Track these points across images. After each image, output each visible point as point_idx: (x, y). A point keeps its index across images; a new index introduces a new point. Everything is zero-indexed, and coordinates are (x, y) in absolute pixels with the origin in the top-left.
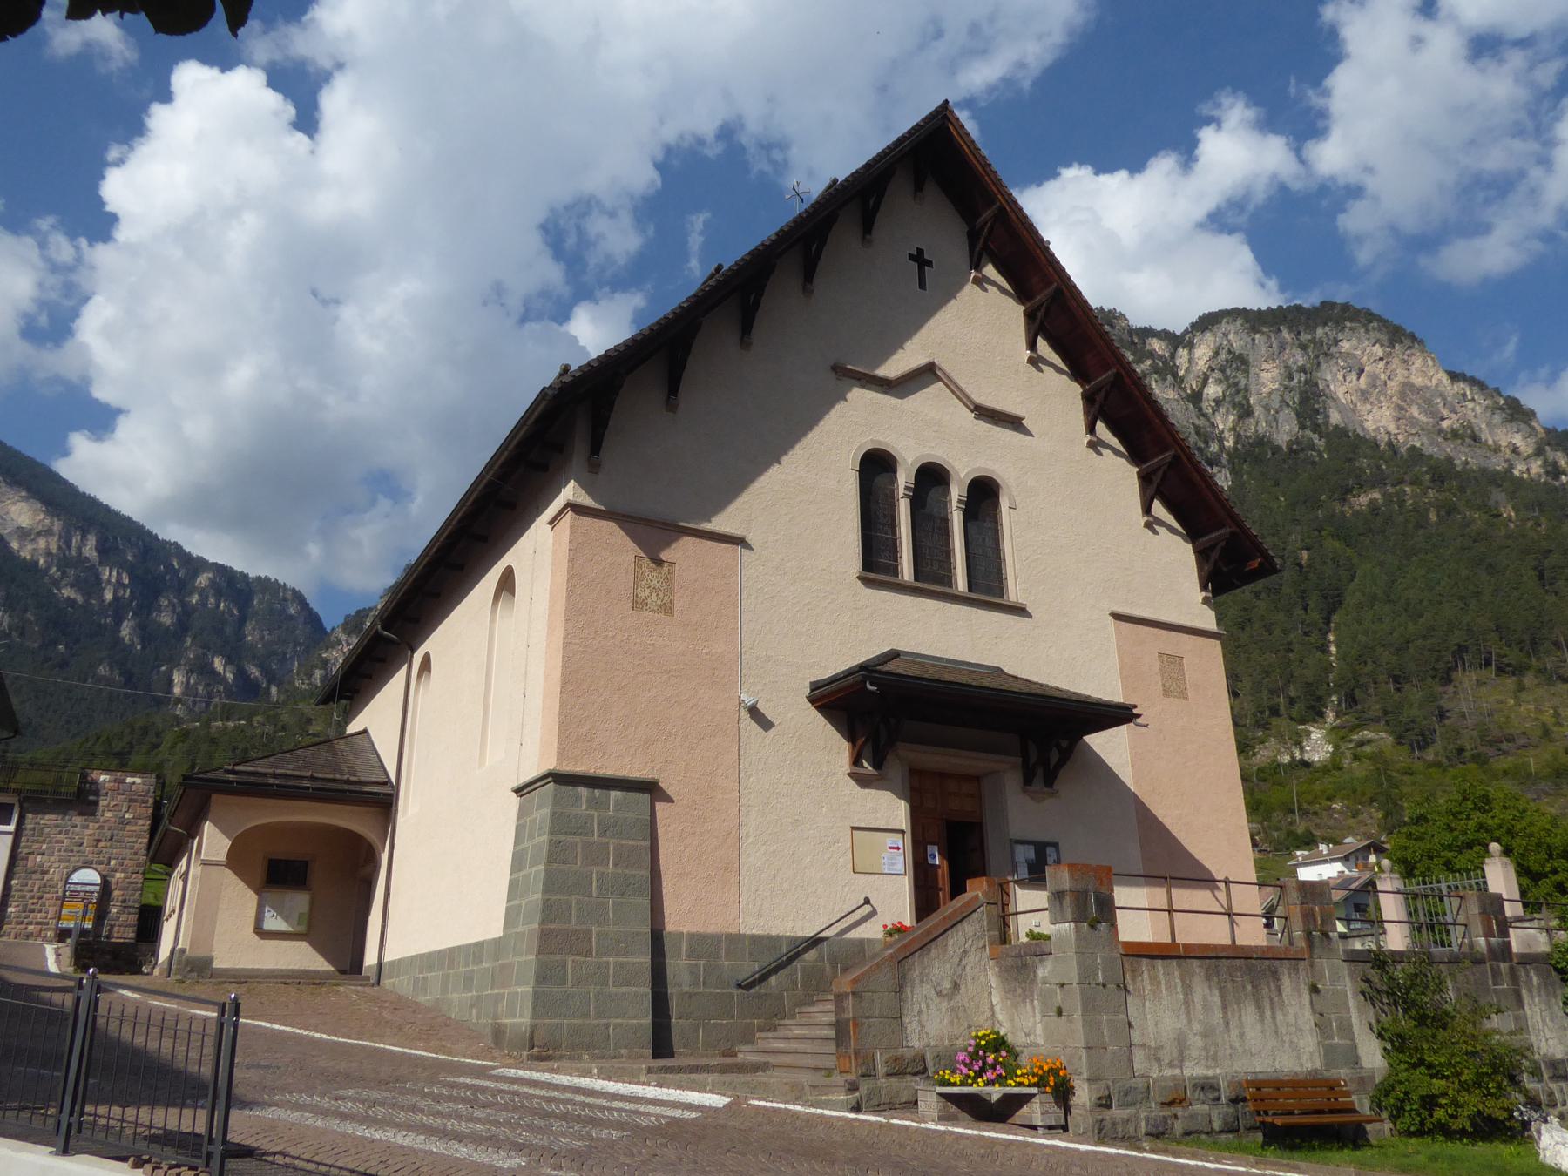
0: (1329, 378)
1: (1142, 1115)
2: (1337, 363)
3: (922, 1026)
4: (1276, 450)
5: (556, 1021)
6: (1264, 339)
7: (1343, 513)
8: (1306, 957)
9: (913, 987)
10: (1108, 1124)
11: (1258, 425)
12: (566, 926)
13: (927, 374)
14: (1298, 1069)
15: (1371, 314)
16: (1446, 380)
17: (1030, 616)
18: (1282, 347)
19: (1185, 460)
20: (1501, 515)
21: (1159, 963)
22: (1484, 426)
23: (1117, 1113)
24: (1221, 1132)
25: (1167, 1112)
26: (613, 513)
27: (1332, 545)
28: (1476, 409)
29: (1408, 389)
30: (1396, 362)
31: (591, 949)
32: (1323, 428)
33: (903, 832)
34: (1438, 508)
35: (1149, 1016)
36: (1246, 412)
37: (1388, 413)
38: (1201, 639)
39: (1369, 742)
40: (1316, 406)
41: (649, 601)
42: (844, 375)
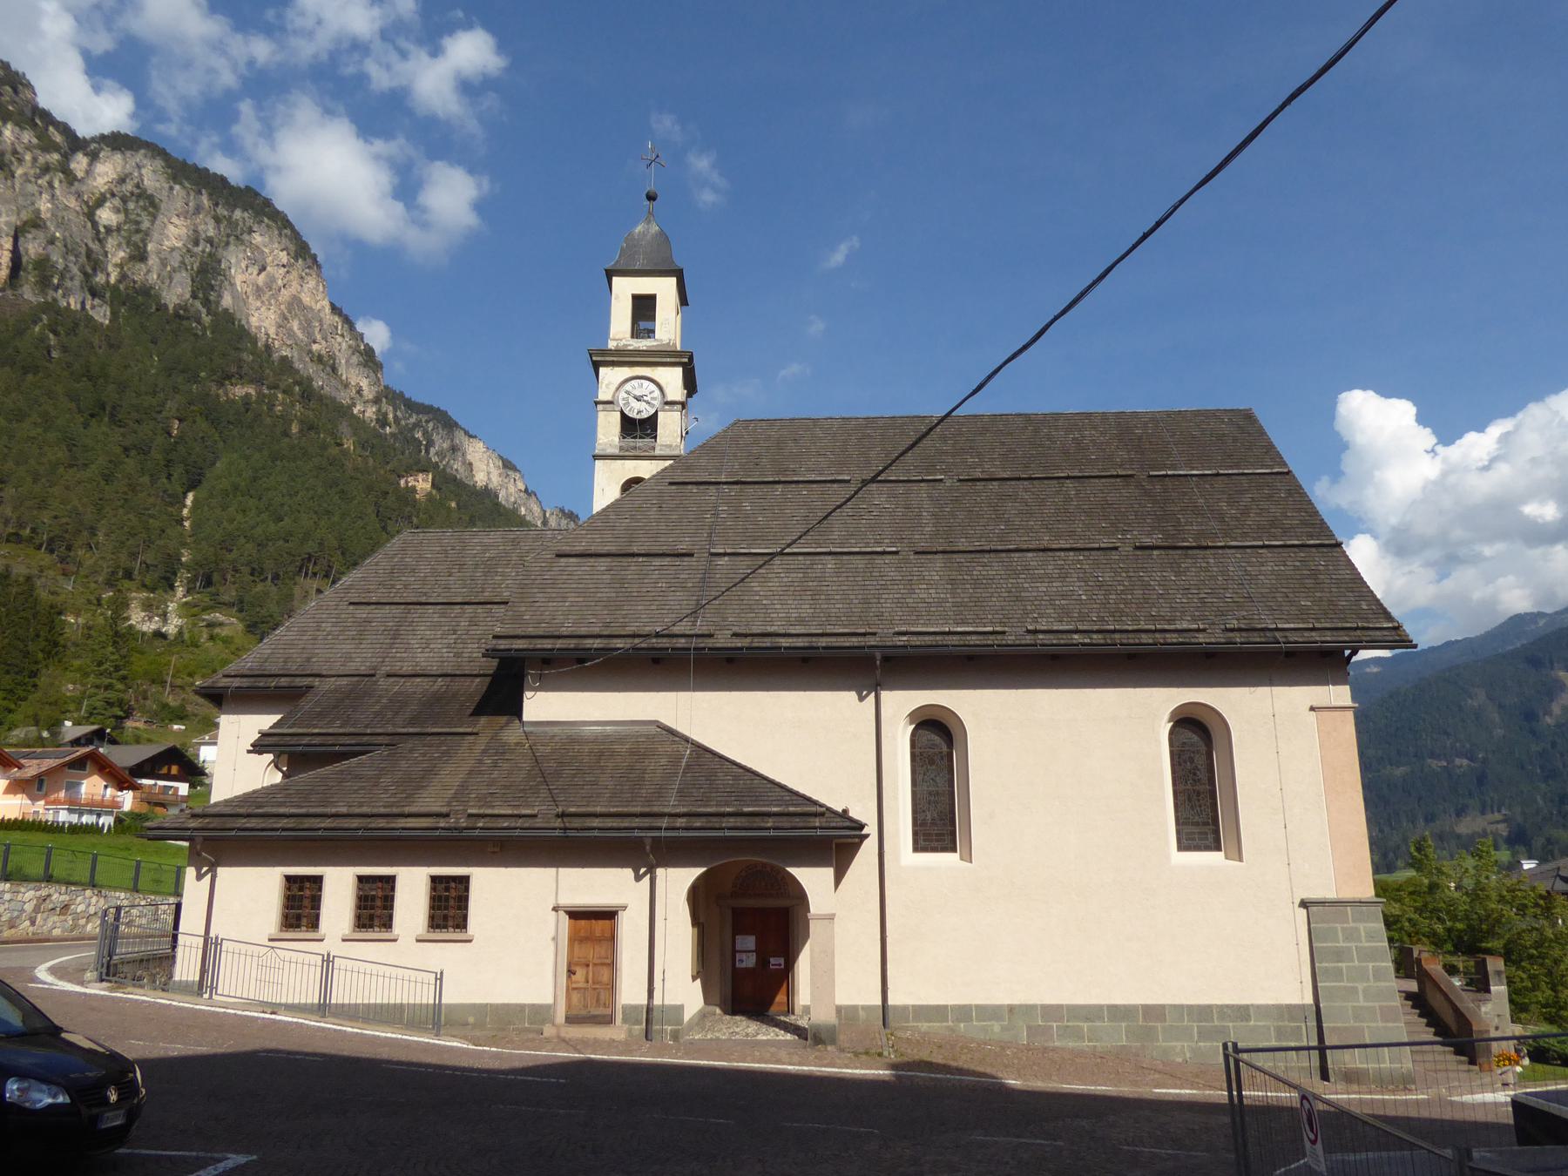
0: (233, 261)
2: (245, 251)
4: (162, 308)
6: (183, 193)
7: (218, 396)
11: (148, 274)
15: (288, 221)
16: (328, 310)
18: (198, 209)
20: (342, 445)
22: (343, 361)
27: (203, 425)
28: (341, 346)
29: (296, 302)
30: (294, 274)
32: (213, 306)
34: (301, 422)
36: (140, 256)
37: (273, 317)
39: (221, 624)
40: (213, 282)
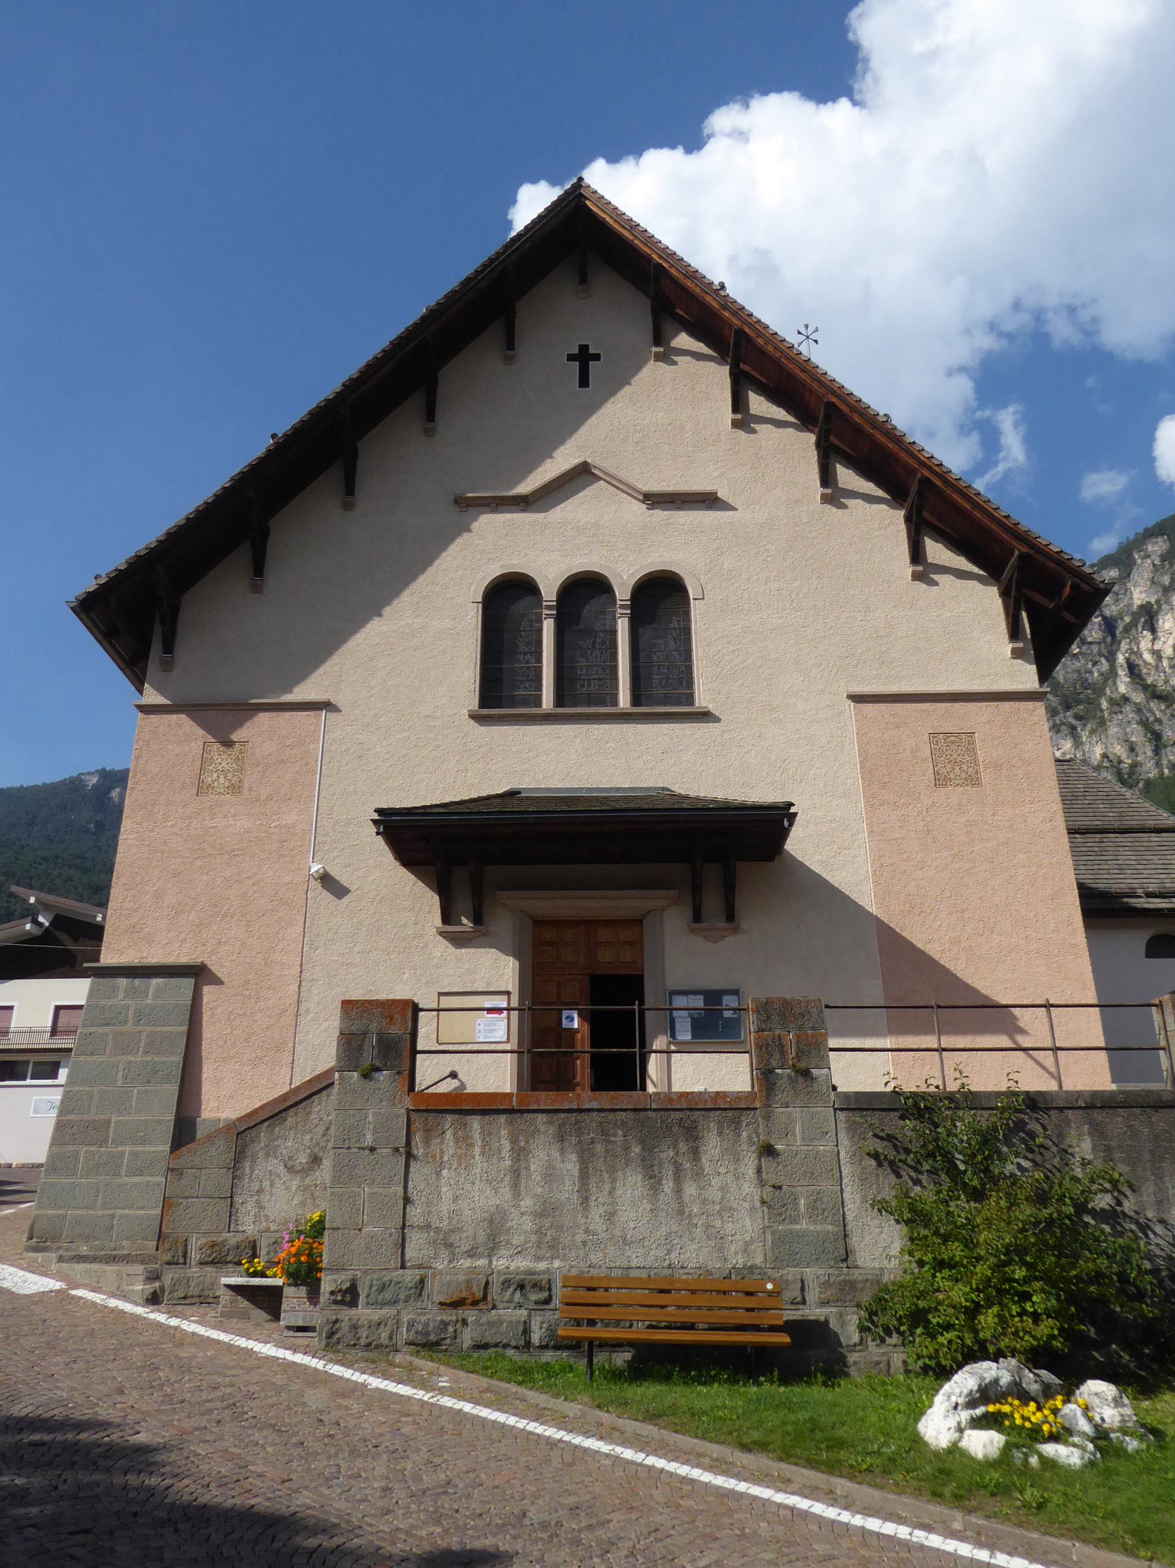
1: (405, 1319)
3: (262, 1208)
5: (60, 1212)
8: (757, 1104)
9: (253, 1162)
10: (345, 1326)
12: (85, 1117)
13: (582, 475)
14: (715, 1264)
17: (715, 719)
19: (938, 483)
21: (475, 1123)
23: (363, 1313)
24: (543, 1347)
25: (450, 1316)
26: (182, 706)
31: (108, 1137)
33: (508, 993)
35: (444, 1189)
38: (1006, 706)
41: (216, 784)
42: (468, 506)
